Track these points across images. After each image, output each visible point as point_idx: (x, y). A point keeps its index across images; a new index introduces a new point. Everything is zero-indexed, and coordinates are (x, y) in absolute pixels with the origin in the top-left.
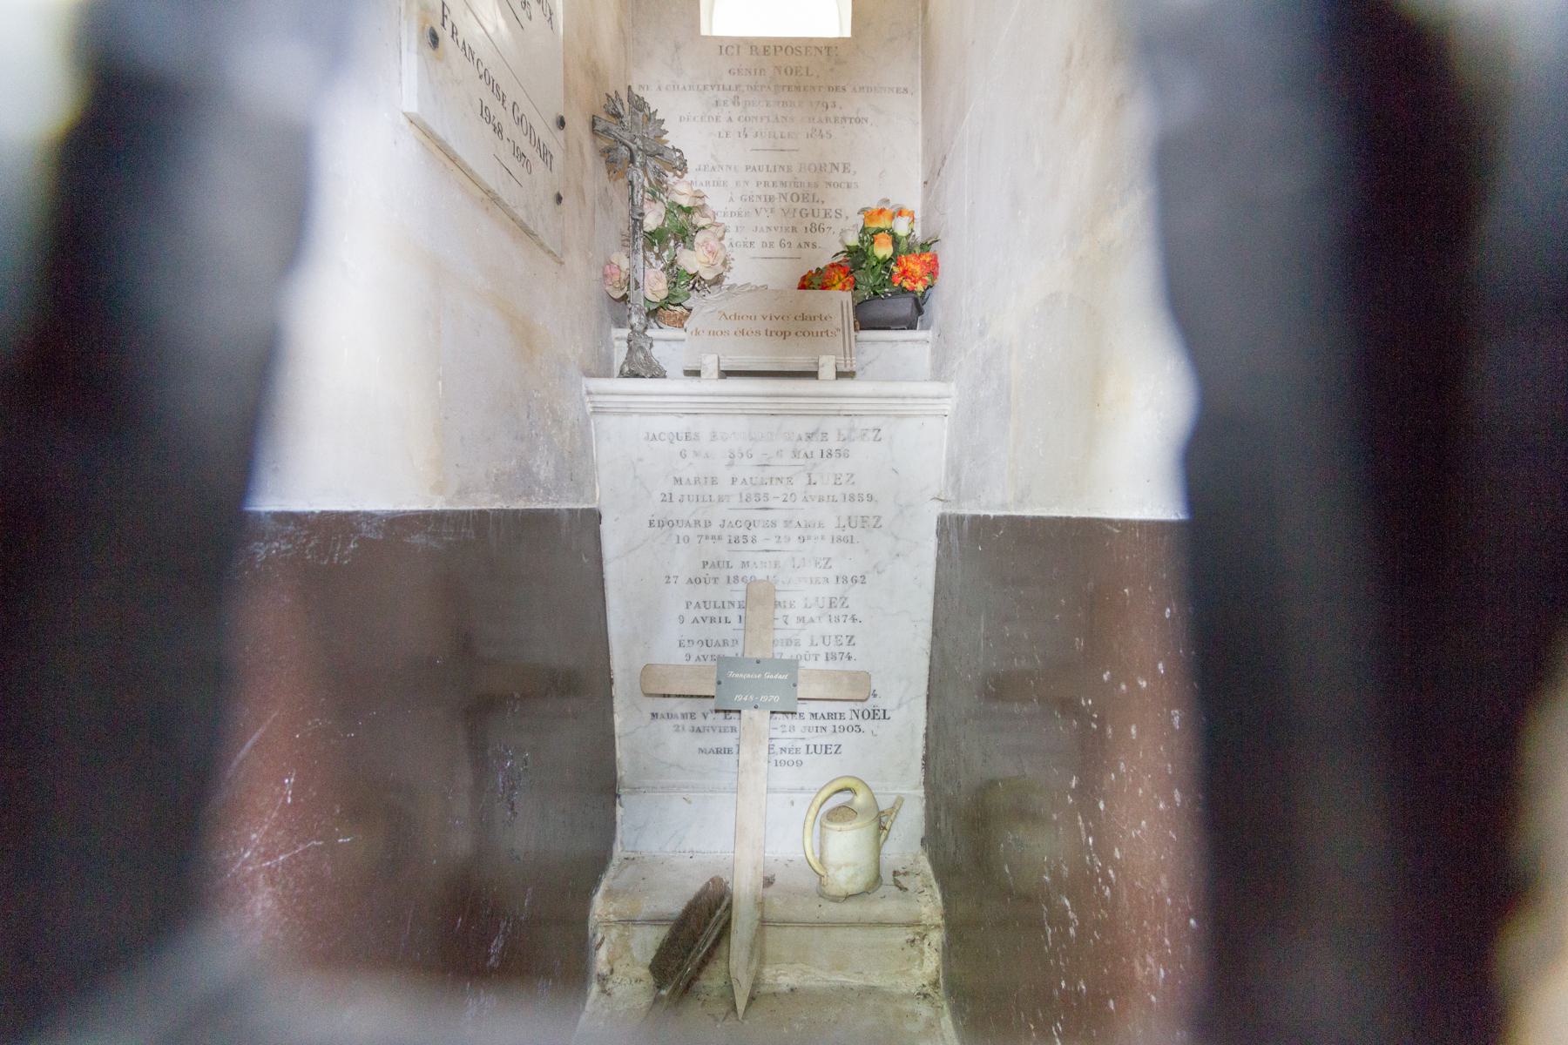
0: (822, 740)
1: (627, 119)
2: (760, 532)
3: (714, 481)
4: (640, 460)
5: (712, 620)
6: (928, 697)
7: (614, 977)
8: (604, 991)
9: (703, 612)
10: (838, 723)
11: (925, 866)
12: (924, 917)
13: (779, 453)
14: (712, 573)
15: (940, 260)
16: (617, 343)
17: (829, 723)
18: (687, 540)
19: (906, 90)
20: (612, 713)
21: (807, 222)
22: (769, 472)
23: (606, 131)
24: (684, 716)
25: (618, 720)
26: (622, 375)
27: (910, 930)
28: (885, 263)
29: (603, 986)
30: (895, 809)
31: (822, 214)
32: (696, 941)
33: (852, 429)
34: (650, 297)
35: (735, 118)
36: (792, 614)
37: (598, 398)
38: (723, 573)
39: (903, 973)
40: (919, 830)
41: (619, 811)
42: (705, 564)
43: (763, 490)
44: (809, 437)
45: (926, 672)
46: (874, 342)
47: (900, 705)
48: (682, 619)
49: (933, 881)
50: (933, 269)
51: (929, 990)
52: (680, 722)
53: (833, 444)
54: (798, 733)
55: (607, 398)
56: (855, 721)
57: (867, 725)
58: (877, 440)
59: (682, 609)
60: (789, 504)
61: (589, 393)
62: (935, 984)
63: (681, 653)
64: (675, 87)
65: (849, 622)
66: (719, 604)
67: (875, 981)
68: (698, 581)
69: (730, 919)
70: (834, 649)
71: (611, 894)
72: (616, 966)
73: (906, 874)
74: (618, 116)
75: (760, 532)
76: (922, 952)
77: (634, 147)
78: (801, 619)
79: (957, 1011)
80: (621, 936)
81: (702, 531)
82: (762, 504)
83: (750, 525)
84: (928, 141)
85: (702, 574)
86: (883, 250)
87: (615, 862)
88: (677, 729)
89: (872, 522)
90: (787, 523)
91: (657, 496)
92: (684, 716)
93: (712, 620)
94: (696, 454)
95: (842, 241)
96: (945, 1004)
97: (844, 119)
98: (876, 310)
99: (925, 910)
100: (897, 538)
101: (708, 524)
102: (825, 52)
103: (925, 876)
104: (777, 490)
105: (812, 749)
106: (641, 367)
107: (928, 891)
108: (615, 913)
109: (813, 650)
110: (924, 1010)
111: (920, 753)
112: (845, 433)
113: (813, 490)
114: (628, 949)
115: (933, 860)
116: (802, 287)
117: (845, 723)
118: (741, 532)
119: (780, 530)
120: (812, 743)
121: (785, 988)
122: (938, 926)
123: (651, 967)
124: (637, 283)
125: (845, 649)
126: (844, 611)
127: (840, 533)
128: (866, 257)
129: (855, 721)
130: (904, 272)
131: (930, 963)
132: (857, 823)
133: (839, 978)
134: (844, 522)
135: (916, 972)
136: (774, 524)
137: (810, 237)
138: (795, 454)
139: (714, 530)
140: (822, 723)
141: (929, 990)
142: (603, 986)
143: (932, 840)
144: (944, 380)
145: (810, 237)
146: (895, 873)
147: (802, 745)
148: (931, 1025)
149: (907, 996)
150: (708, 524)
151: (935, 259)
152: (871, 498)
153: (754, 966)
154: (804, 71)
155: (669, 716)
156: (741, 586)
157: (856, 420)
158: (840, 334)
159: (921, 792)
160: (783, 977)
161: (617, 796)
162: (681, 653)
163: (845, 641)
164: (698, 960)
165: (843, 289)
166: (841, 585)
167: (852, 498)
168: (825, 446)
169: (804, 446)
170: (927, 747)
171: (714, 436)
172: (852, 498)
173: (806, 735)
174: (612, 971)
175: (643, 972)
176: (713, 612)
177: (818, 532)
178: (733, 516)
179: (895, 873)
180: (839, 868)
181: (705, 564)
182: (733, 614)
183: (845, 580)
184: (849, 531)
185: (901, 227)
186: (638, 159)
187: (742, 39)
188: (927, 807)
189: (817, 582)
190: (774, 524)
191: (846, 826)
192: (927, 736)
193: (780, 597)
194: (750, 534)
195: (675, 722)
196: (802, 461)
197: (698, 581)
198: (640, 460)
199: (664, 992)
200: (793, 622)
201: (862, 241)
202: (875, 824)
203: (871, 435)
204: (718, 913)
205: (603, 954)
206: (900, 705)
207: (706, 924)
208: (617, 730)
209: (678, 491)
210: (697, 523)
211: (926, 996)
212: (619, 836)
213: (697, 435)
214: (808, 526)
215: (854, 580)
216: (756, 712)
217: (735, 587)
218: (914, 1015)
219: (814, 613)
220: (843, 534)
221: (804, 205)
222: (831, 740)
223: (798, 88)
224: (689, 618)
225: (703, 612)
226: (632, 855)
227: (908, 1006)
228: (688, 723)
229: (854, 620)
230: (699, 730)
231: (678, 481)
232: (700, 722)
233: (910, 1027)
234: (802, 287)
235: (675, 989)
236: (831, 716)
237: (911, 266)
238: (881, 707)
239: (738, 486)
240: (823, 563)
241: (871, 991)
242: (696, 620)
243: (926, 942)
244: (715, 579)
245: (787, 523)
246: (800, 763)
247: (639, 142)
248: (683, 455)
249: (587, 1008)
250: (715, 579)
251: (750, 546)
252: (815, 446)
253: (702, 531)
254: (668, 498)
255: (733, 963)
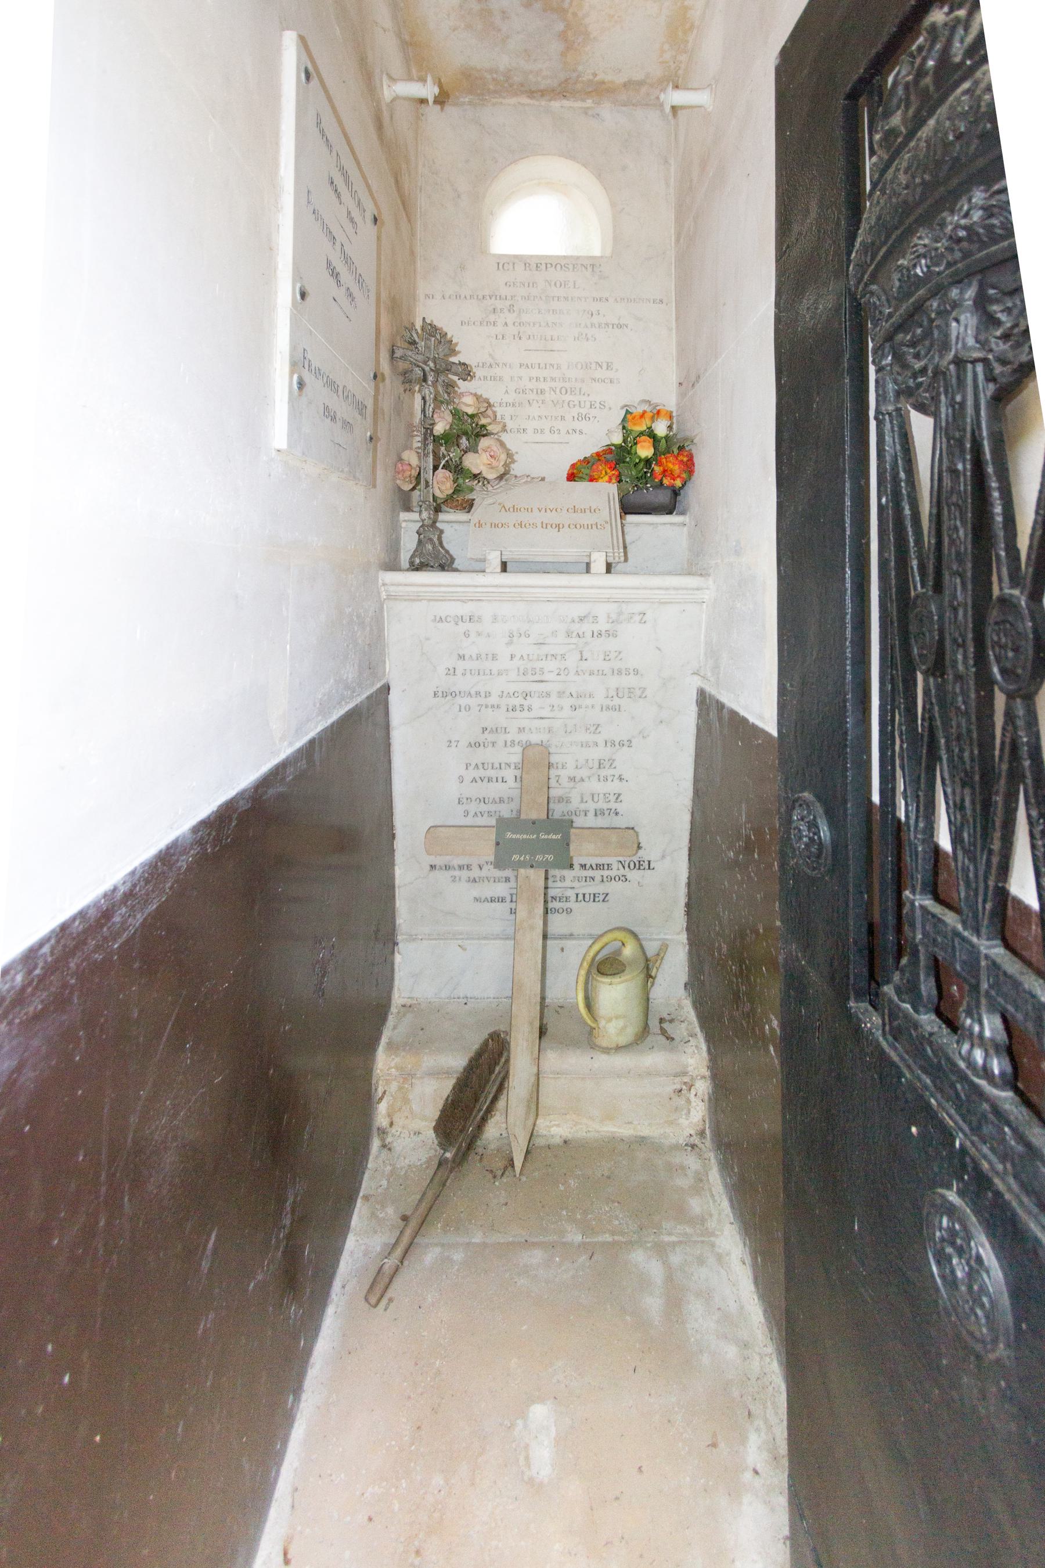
0: (590, 889)
1: (422, 344)
2: (535, 702)
3: (494, 657)
4: (428, 639)
5: (490, 780)
6: (690, 849)
7: (393, 1130)
8: (384, 1146)
9: (481, 773)
10: (606, 873)
11: (690, 1013)
12: (690, 1069)
13: (554, 633)
14: (490, 737)
15: (695, 460)
16: (404, 525)
17: (597, 874)
18: (468, 708)
19: (661, 301)
20: (393, 865)
21: (575, 412)
22: (545, 649)
23: (403, 358)
24: (461, 867)
25: (398, 872)
26: (416, 567)
27: (677, 1080)
28: (648, 462)
29: (383, 1140)
30: (660, 955)
31: (588, 404)
32: (476, 1100)
33: (620, 613)
34: (438, 494)
35: (510, 323)
36: (564, 774)
37: (392, 588)
38: (501, 738)
39: (671, 1123)
40: (683, 976)
41: (398, 958)
42: (484, 729)
43: (538, 665)
44: (581, 620)
45: (688, 826)
46: (637, 524)
47: (663, 857)
48: (461, 779)
49: (698, 1030)
50: (689, 466)
51: (696, 1140)
52: (457, 873)
53: (603, 625)
54: (568, 883)
55: (401, 588)
56: (622, 872)
57: (634, 875)
58: (643, 622)
59: (462, 771)
60: (562, 677)
61: (384, 585)
62: (702, 1134)
63: (461, 809)
64: (458, 297)
65: (616, 781)
66: (497, 765)
67: (645, 1131)
68: (477, 745)
69: (508, 1072)
70: (602, 805)
71: (391, 1046)
72: (395, 1119)
73: (671, 1021)
74: (413, 343)
75: (535, 702)
76: (688, 1101)
77: (427, 369)
78: (572, 779)
79: (725, 1167)
80: (400, 1088)
81: (482, 700)
82: (537, 678)
83: (526, 695)
84: (683, 351)
85: (481, 738)
86: (645, 451)
87: (393, 1010)
88: (454, 879)
89: (638, 693)
90: (561, 694)
91: (441, 670)
92: (461, 867)
93: (490, 780)
94: (479, 634)
95: (679, 934)
96: (712, 1155)
97: (607, 324)
98: (636, 499)
99: (691, 1061)
100: (660, 707)
101: (488, 694)
102: (590, 269)
103: (690, 1023)
104: (552, 665)
105: (580, 897)
106: (433, 558)
107: (693, 1042)
108: (397, 1068)
109: (583, 806)
110: (692, 1162)
111: (683, 900)
112: (614, 616)
113: (584, 665)
114: (406, 1101)
115: (698, 1005)
116: (571, 477)
117: (613, 873)
118: (517, 701)
119: (554, 700)
120: (581, 891)
121: (558, 1141)
122: (704, 1077)
123: (436, 1129)
124: (427, 482)
125: (613, 805)
126: (612, 772)
127: (608, 702)
128: (629, 453)
129: (622, 872)
130: (665, 471)
131: (697, 1113)
132: (626, 976)
133: (609, 1129)
134: (612, 693)
135: (683, 1121)
136: (548, 695)
137: (578, 425)
138: (569, 634)
139: (493, 700)
140: (590, 873)
141: (696, 1140)
142: (383, 1140)
143: (696, 984)
144: (703, 574)
145: (578, 425)
146: (662, 1021)
147: (571, 894)
148: (700, 1179)
149: (676, 1147)
150: (488, 694)
151: (691, 458)
152: (636, 672)
153: (530, 1122)
154: (571, 284)
155: (447, 868)
156: (518, 749)
157: (624, 606)
158: (608, 526)
159: (683, 937)
160: (555, 1128)
161: (395, 944)
162: (461, 809)
163: (613, 798)
164: (479, 1117)
165: (610, 481)
166: (609, 749)
167: (620, 672)
168: (596, 628)
169: (576, 627)
170: (689, 895)
171: (495, 619)
172: (620, 672)
173: (576, 884)
174: (391, 1124)
175: (431, 1134)
176: (491, 773)
177: (588, 702)
178: (512, 688)
179: (662, 1021)
180: (610, 1020)
181: (484, 729)
182: (509, 774)
183: (613, 744)
184: (616, 701)
185: (661, 429)
186: (430, 379)
187: (516, 257)
188: (690, 953)
189: (588, 745)
190: (548, 695)
191: (616, 979)
192: (689, 885)
193: (553, 759)
194: (526, 703)
195: (452, 873)
196: (574, 640)
197: (477, 745)
198: (428, 639)
199: (448, 1155)
200: (564, 781)
201: (625, 441)
202: (642, 976)
203: (637, 618)
204: (497, 1069)
205: (382, 1108)
206: (663, 857)
207: (487, 1081)
208: (397, 882)
209: (461, 665)
210: (478, 694)
211: (693, 1146)
212: (396, 983)
213: (480, 618)
214: (579, 696)
215: (621, 744)
216: (532, 871)
217: (512, 750)
218: (683, 1168)
219: (584, 773)
220: (611, 704)
221: (571, 398)
222: (600, 889)
223: (566, 299)
224: (468, 779)
225: (481, 773)
226: (409, 1002)
227: (678, 1159)
228: (465, 874)
229: (621, 779)
230: (474, 881)
231: (462, 657)
232: (475, 873)
233: (682, 1182)
234: (571, 477)
235: (458, 1150)
236: (599, 867)
237: (670, 466)
238: (646, 859)
239: (517, 662)
240: (593, 729)
241: (642, 1140)
242: (474, 780)
243: (693, 1092)
244: (493, 744)
245: (561, 694)
246: (569, 911)
247: (431, 364)
248: (467, 635)
249: (369, 1166)
250: (493, 744)
251: (526, 714)
252: (587, 628)
253: (482, 700)
254: (452, 672)
255: (511, 1119)
